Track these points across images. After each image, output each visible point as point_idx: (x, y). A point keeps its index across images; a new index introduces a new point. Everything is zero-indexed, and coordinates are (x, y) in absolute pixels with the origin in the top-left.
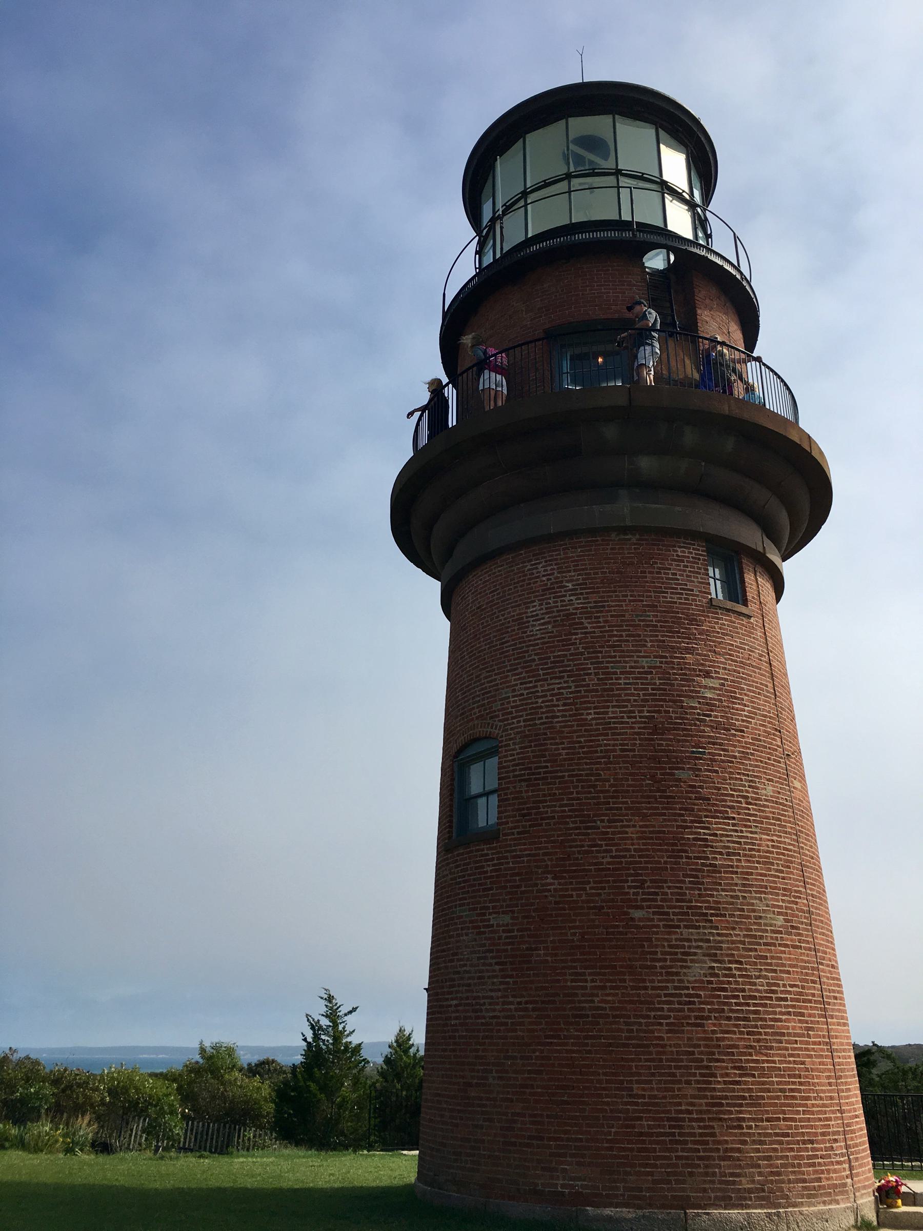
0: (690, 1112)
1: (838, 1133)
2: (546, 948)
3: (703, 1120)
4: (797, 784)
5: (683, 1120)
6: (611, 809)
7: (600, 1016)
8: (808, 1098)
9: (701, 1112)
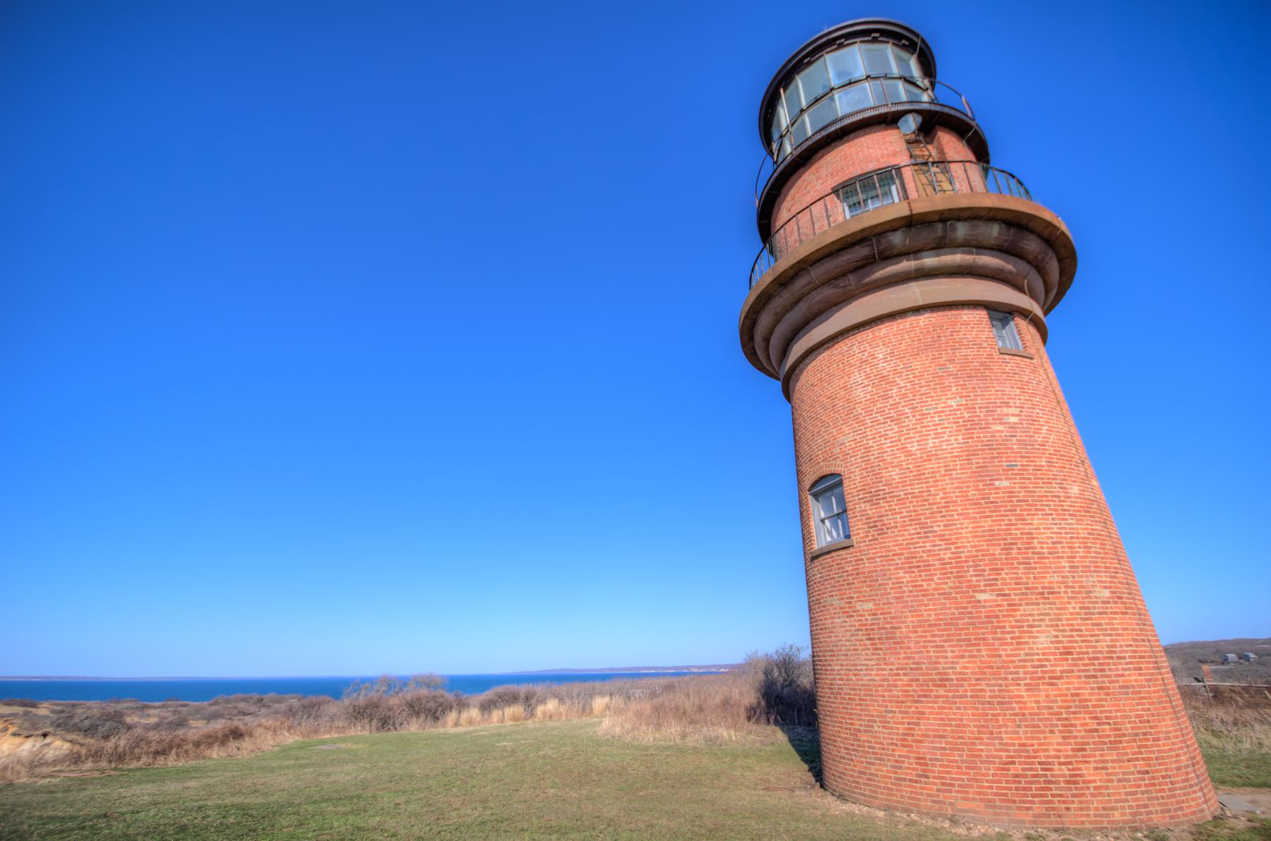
2: (908, 627)
3: (1070, 763)
9: (1067, 757)
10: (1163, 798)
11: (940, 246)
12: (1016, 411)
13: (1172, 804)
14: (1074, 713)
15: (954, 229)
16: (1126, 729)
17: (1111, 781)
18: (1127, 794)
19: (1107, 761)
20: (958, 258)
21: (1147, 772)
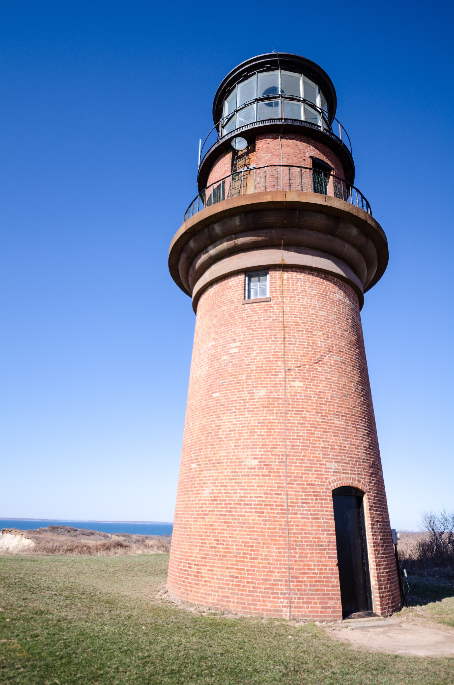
10: (242, 595)
11: (214, 240)
12: (238, 344)
13: (191, 579)
14: (208, 536)
15: (214, 229)
16: (233, 549)
17: (213, 578)
18: (219, 588)
19: (214, 567)
20: (225, 245)
21: (237, 577)
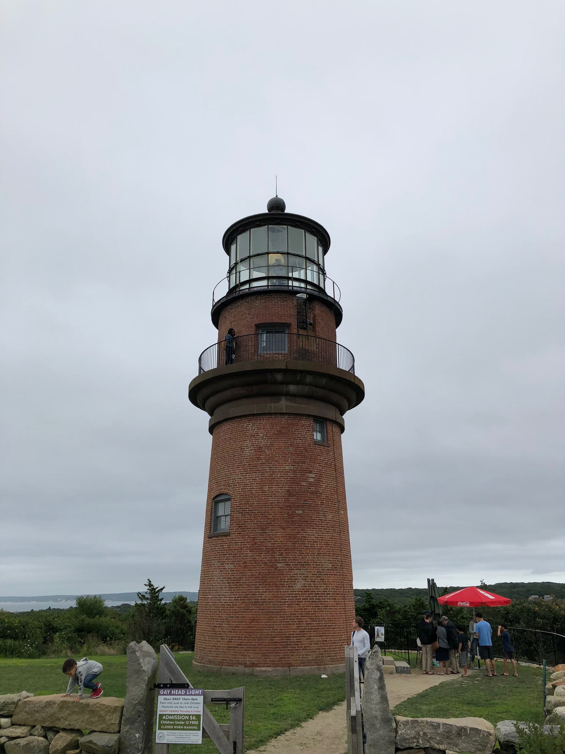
0: (293, 634)
1: (345, 640)
2: (246, 578)
4: (342, 512)
5: (291, 637)
6: (272, 526)
7: (264, 602)
8: (335, 628)
12: (314, 476)
